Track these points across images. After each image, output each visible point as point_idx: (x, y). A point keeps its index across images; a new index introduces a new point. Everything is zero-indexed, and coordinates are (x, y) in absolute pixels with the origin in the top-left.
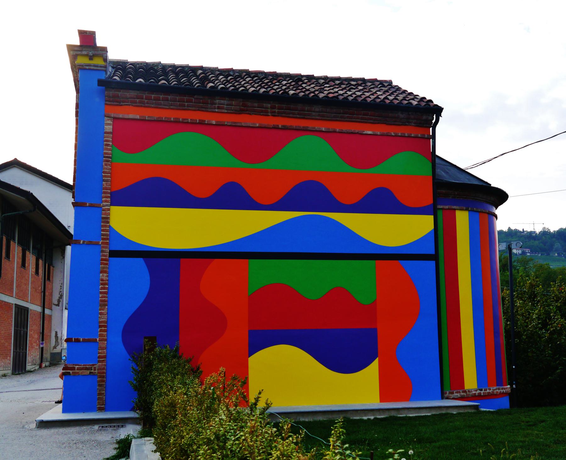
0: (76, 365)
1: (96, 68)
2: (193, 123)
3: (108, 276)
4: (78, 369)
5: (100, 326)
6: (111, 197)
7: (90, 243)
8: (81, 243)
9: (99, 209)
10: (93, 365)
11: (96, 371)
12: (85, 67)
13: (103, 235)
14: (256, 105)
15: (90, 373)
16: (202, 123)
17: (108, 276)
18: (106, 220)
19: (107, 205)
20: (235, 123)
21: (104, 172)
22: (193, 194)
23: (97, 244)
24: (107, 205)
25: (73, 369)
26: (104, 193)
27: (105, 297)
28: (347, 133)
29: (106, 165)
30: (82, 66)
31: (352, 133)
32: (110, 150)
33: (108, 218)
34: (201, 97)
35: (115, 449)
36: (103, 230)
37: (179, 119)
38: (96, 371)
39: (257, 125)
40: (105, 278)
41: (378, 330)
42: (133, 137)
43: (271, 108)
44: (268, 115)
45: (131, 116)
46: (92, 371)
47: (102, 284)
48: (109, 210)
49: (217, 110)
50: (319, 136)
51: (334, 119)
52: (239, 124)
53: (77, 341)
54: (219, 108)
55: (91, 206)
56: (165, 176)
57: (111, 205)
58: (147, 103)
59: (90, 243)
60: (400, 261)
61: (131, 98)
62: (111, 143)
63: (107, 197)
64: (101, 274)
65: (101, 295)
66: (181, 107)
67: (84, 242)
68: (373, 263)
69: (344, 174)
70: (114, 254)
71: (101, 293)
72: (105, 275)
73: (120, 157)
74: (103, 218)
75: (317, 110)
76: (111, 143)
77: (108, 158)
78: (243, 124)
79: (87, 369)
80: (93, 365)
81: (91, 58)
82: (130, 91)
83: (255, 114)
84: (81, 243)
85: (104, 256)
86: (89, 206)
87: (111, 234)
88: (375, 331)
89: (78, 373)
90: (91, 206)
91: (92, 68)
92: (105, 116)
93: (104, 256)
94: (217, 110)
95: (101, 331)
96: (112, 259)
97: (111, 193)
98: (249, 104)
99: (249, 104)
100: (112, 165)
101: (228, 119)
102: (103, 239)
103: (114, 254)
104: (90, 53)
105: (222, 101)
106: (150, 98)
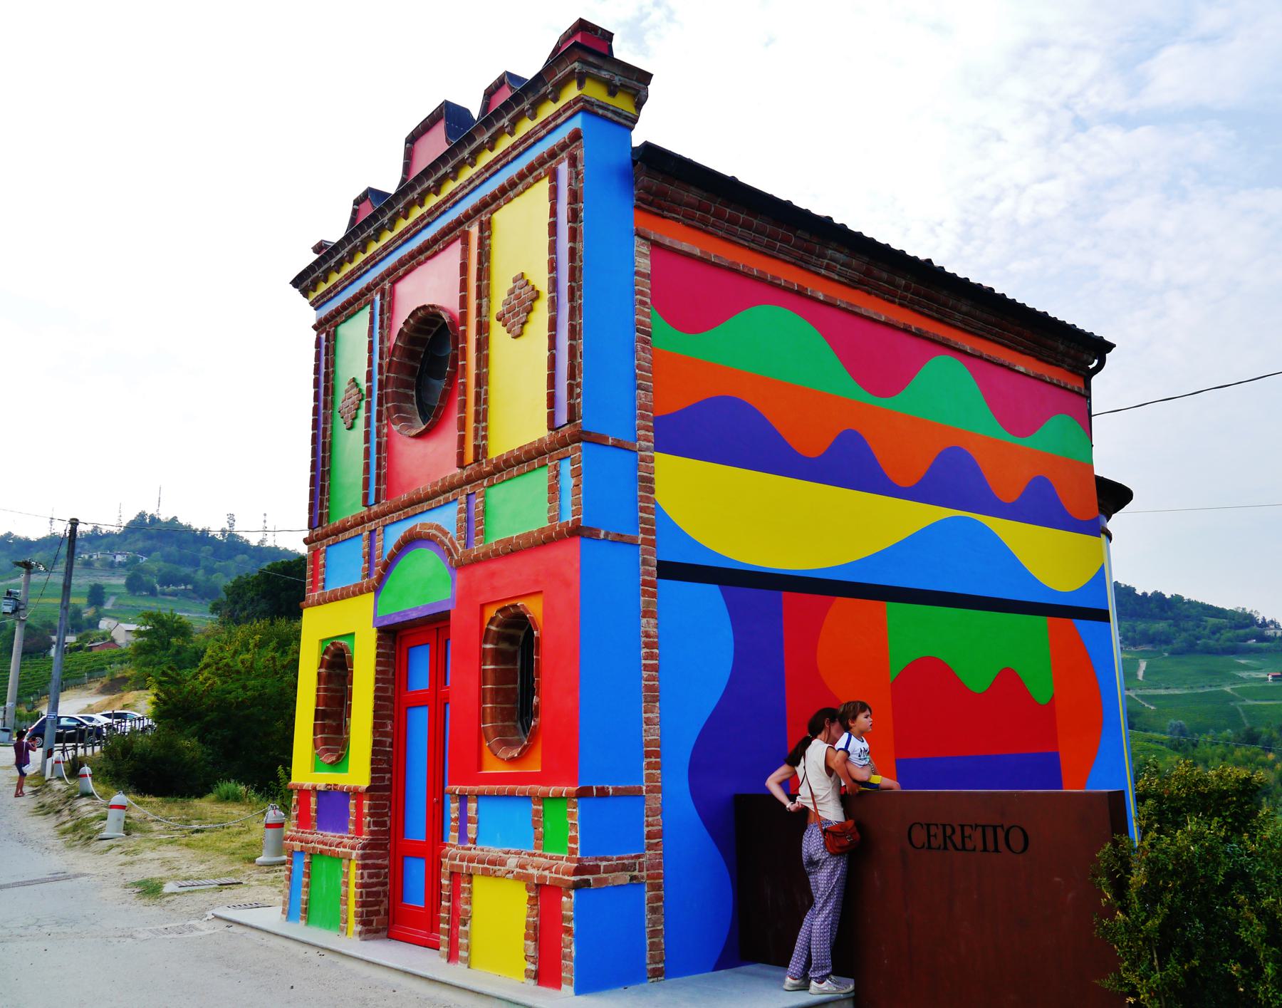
0: (601, 860)
1: (616, 118)
2: (787, 290)
3: (657, 626)
4: (609, 870)
5: (648, 754)
6: (656, 429)
7: (619, 540)
8: (602, 536)
9: (633, 455)
10: (638, 857)
11: (644, 873)
12: (596, 109)
13: (645, 521)
14: (885, 275)
15: (633, 878)
16: (800, 293)
17: (657, 626)
18: (648, 483)
19: (647, 449)
20: (852, 305)
21: (640, 367)
22: (794, 446)
23: (633, 543)
24: (647, 449)
25: (595, 870)
26: (643, 417)
27: (653, 679)
28: (987, 360)
29: (643, 350)
30: (592, 104)
31: (1002, 365)
32: (648, 316)
33: (651, 480)
34: (807, 237)
35: (139, 633)
36: (643, 509)
37: (765, 274)
38: (644, 873)
39: (883, 319)
40: (652, 631)
41: (1061, 757)
42: (690, 297)
43: (907, 288)
44: (893, 302)
45: (685, 246)
46: (636, 873)
47: (647, 645)
48: (652, 460)
49: (823, 272)
50: (966, 365)
51: (981, 333)
52: (857, 310)
53: (603, 793)
54: (828, 268)
55: (618, 446)
56: (749, 398)
57: (657, 449)
58: (713, 225)
59: (619, 540)
60: (1076, 621)
61: (687, 205)
62: (648, 301)
63: (647, 429)
64: (644, 621)
65: (645, 674)
66: (768, 252)
67: (607, 534)
68: (1041, 622)
69: (860, 404)
70: (668, 570)
71: (647, 667)
72: (652, 621)
73: (667, 337)
74: (643, 479)
75: (964, 309)
76: (648, 301)
77: (645, 333)
78: (863, 311)
79: (624, 868)
80: (638, 857)
81: (612, 93)
82: (692, 188)
83: (877, 296)
84: (602, 536)
85: (649, 574)
86: (613, 446)
87: (655, 523)
88: (1056, 756)
89: (606, 880)
90: (618, 446)
91: (610, 115)
92: (638, 234)
93: (649, 574)
94: (823, 272)
95: (649, 766)
96: (664, 583)
97: (656, 420)
98: (876, 271)
99: (876, 271)
100: (654, 352)
101: (844, 297)
102: (645, 531)
103: (668, 570)
104: (617, 78)
105: (838, 255)
106: (719, 215)
